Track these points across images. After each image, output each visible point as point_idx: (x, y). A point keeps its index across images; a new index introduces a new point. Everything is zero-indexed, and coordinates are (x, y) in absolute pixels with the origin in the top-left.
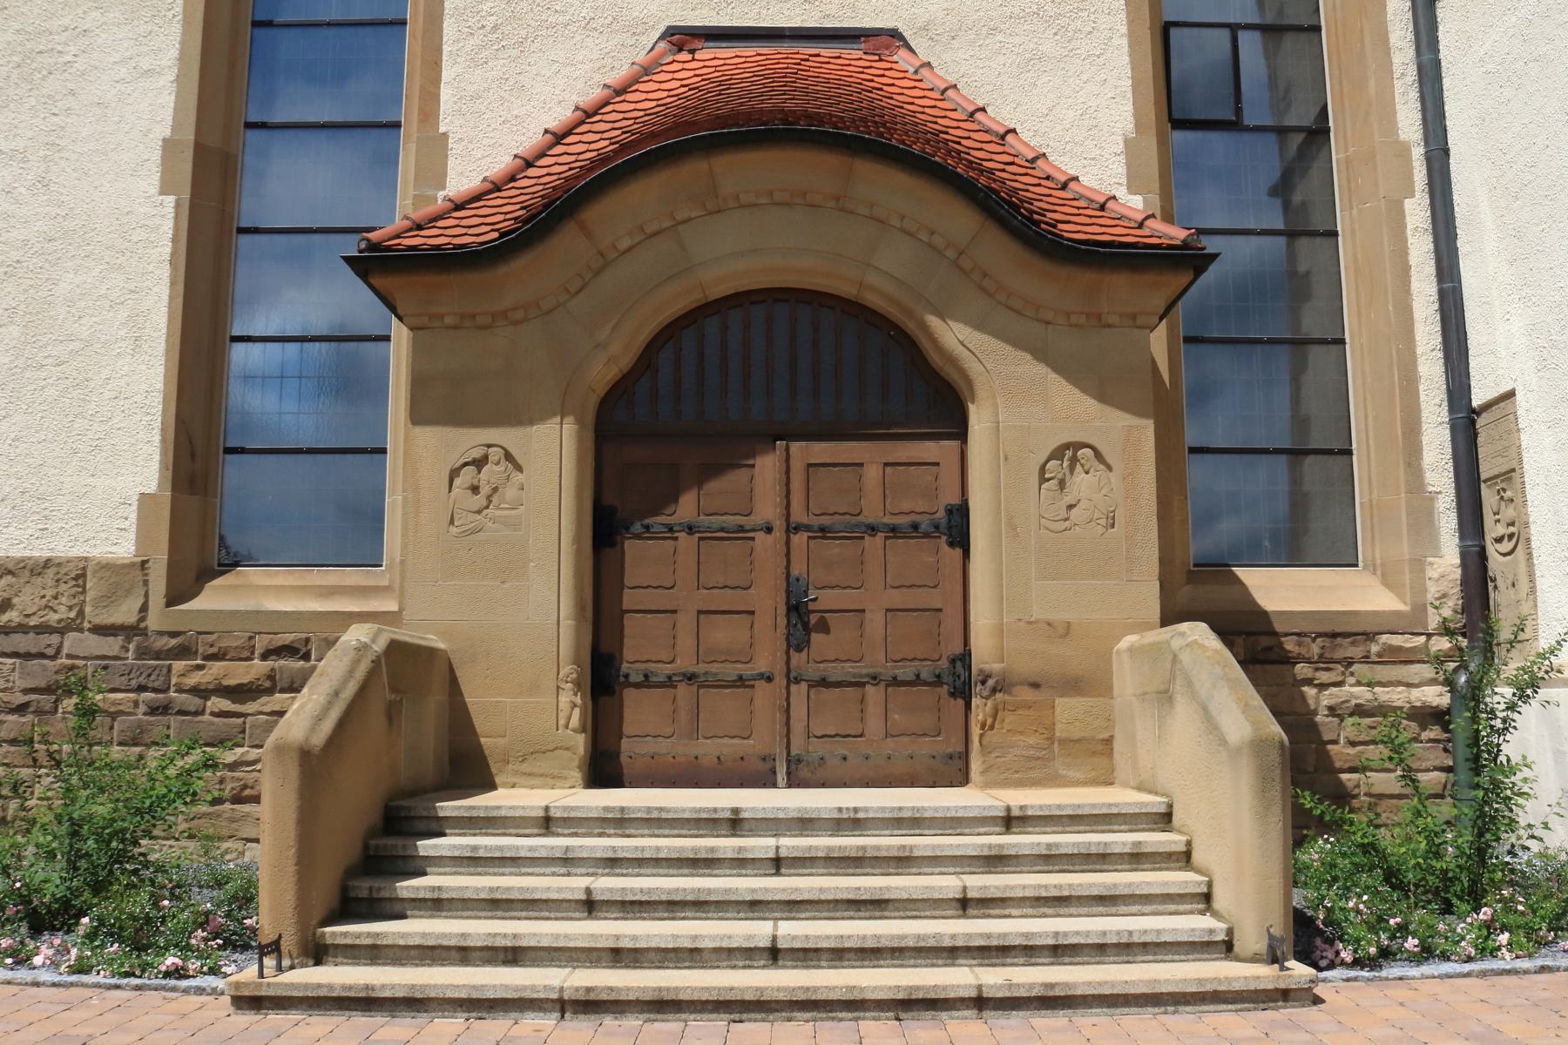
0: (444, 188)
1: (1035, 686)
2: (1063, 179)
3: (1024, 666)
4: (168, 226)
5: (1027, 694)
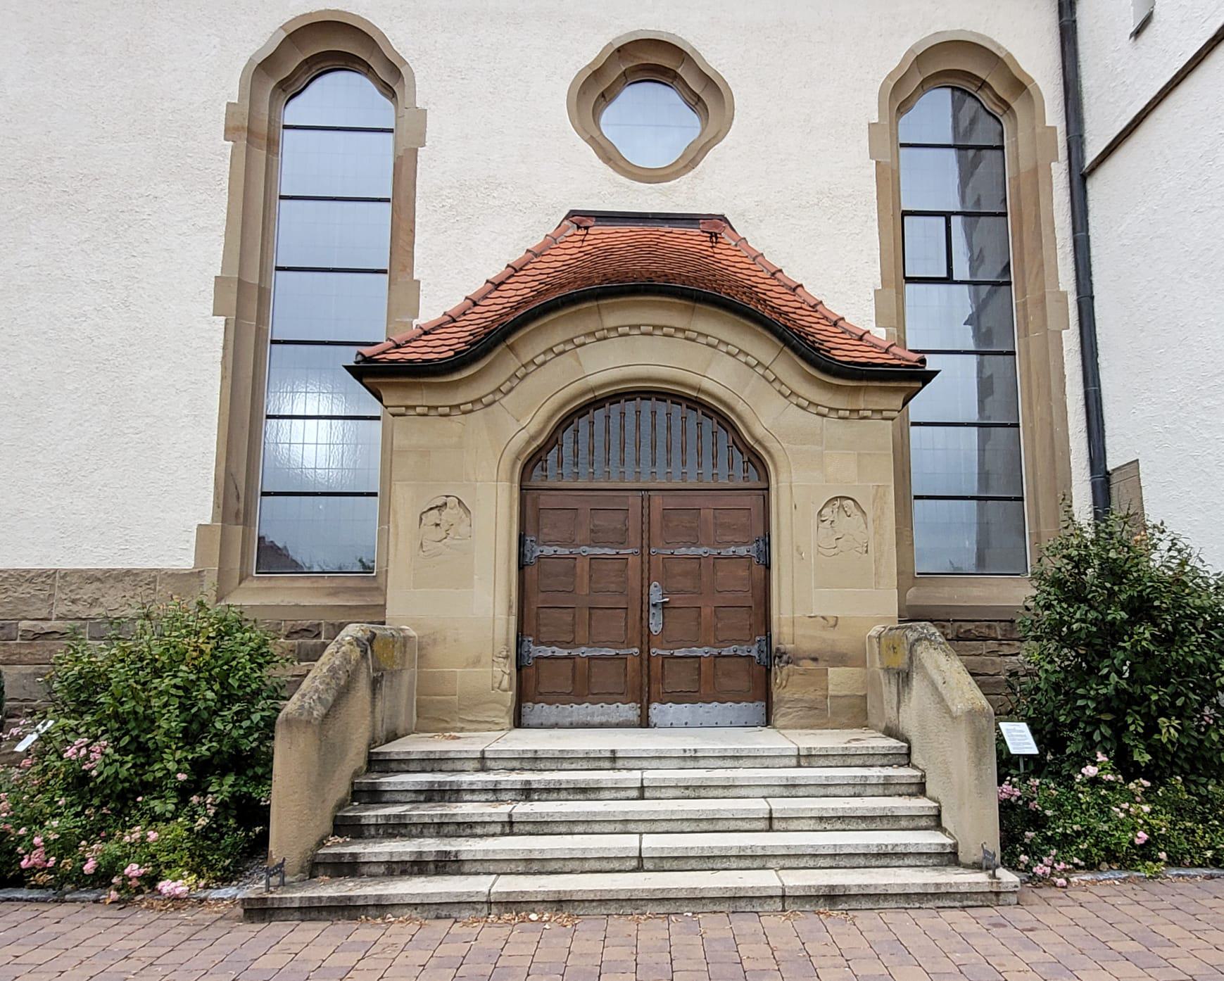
0: (417, 317)
1: (815, 659)
2: (834, 319)
3: (807, 646)
4: (220, 337)
5: (810, 665)
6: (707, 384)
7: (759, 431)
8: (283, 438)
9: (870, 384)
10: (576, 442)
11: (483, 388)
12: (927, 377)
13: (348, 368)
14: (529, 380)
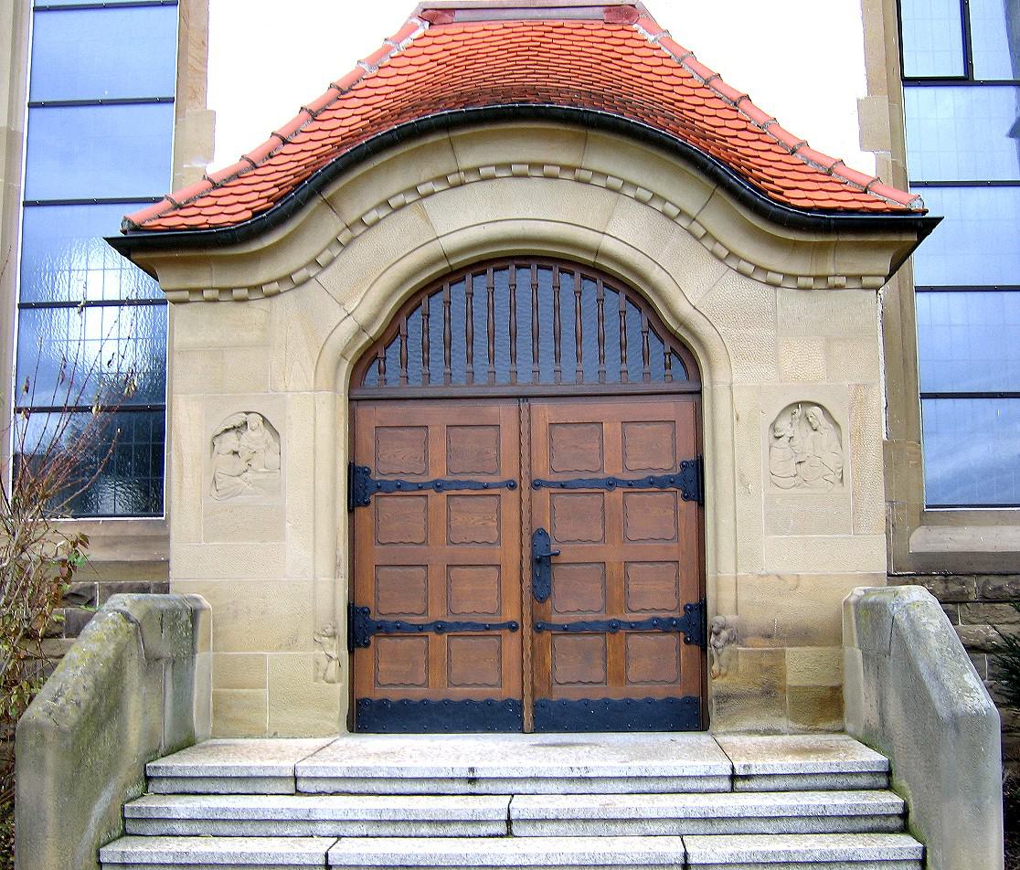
6: (609, 245)
7: (684, 308)
8: (75, 333)
9: (842, 239)
10: (426, 331)
11: (292, 261)
12: (922, 226)
13: (113, 242)
14: (356, 249)
